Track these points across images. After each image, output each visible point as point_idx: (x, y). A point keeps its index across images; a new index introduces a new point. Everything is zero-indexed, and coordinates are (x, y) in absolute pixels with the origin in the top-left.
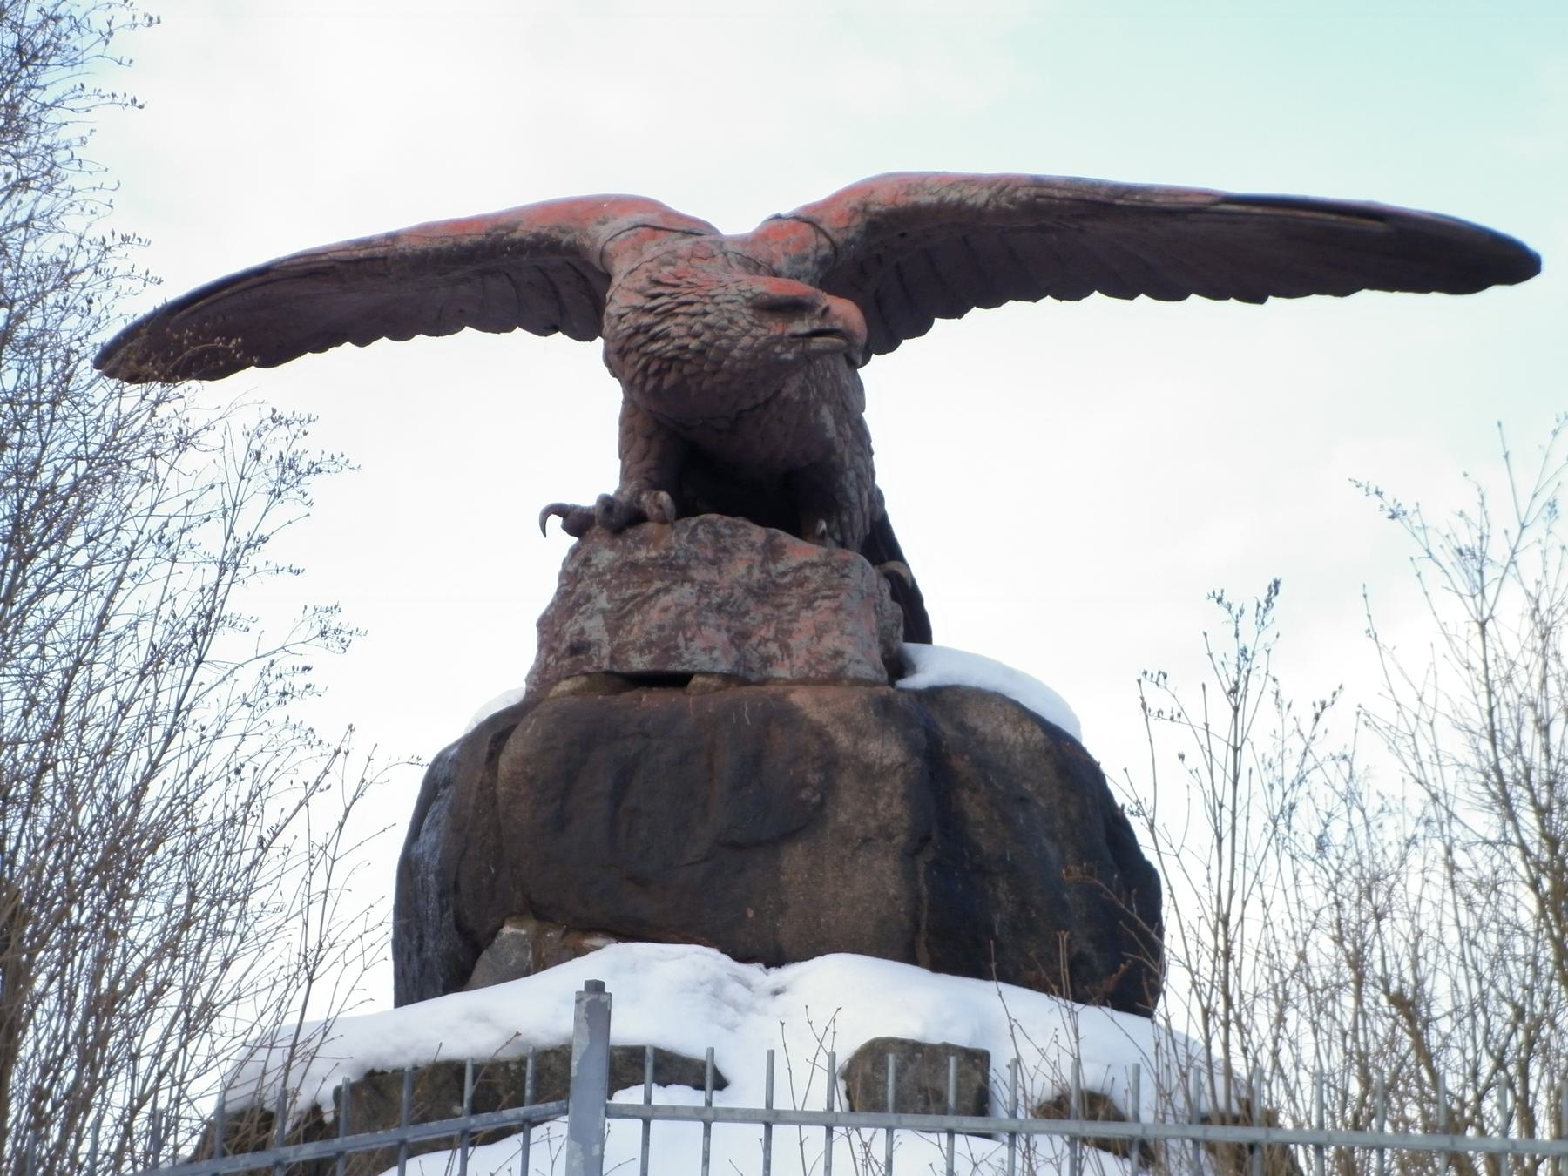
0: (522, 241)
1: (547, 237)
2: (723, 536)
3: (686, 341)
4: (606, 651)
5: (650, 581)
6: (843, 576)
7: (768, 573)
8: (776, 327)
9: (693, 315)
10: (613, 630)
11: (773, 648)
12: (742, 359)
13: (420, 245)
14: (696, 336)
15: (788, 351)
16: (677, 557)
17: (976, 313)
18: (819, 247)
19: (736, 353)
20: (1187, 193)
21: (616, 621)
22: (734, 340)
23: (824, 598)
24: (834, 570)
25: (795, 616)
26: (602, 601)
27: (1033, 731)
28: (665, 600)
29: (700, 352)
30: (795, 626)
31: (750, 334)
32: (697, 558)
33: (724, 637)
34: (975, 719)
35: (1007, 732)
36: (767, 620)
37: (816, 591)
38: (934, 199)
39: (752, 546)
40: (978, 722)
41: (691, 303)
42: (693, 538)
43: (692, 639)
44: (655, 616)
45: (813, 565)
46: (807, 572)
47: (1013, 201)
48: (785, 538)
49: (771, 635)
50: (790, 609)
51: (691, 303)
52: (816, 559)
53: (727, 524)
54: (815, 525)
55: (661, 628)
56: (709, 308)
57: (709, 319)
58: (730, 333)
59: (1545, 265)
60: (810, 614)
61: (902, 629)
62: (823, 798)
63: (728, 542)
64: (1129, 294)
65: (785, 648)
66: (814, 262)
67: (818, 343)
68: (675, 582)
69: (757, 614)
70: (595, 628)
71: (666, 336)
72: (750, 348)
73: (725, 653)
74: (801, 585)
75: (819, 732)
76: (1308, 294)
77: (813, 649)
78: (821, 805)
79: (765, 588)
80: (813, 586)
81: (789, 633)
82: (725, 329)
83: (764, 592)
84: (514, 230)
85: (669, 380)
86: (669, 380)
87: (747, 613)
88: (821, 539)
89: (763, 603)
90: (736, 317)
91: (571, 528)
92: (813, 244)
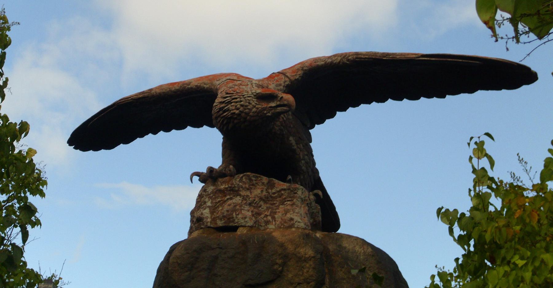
0: (192, 88)
1: (200, 86)
2: (252, 180)
3: (235, 111)
4: (209, 220)
5: (225, 196)
6: (296, 193)
7: (268, 192)
8: (264, 105)
9: (237, 102)
10: (212, 213)
11: (269, 218)
12: (253, 116)
13: (158, 91)
14: (238, 109)
15: (269, 113)
16: (235, 187)
17: (350, 109)
18: (285, 82)
19: (251, 114)
20: (408, 54)
21: (213, 210)
22: (250, 110)
23: (288, 201)
24: (292, 191)
25: (278, 207)
26: (209, 204)
27: (368, 249)
28: (230, 202)
29: (239, 115)
30: (278, 210)
31: (256, 106)
32: (242, 187)
33: (250, 213)
34: (345, 244)
35: (357, 248)
36: (268, 208)
37: (285, 198)
38: (323, 63)
39: (263, 183)
40: (347, 245)
41: (236, 98)
42: (241, 180)
43: (238, 215)
44: (226, 207)
45: (284, 190)
46: (283, 192)
47: (348, 60)
48: (276, 181)
49: (268, 214)
50: (276, 205)
51: (236, 98)
52: (285, 187)
53: (253, 176)
54: (286, 178)
55: (228, 211)
56: (242, 99)
57: (242, 103)
58: (249, 107)
59: (539, 76)
60: (283, 206)
61: (320, 213)
62: (283, 268)
63: (254, 182)
64: (401, 99)
65: (274, 218)
66: (284, 86)
67: (279, 109)
68: (234, 196)
69: (264, 206)
70: (206, 212)
71: (228, 110)
72: (256, 112)
73: (251, 219)
74: (280, 197)
75: (282, 245)
76: (460, 93)
77: (283, 218)
78: (281, 272)
79: (268, 198)
80: (284, 197)
81: (275, 213)
82: (247, 106)
83: (265, 200)
84: (189, 85)
85: (231, 125)
86: (231, 125)
87: (260, 206)
88: (289, 182)
89: (267, 203)
90: (251, 102)
91: (201, 180)
92: (283, 80)
